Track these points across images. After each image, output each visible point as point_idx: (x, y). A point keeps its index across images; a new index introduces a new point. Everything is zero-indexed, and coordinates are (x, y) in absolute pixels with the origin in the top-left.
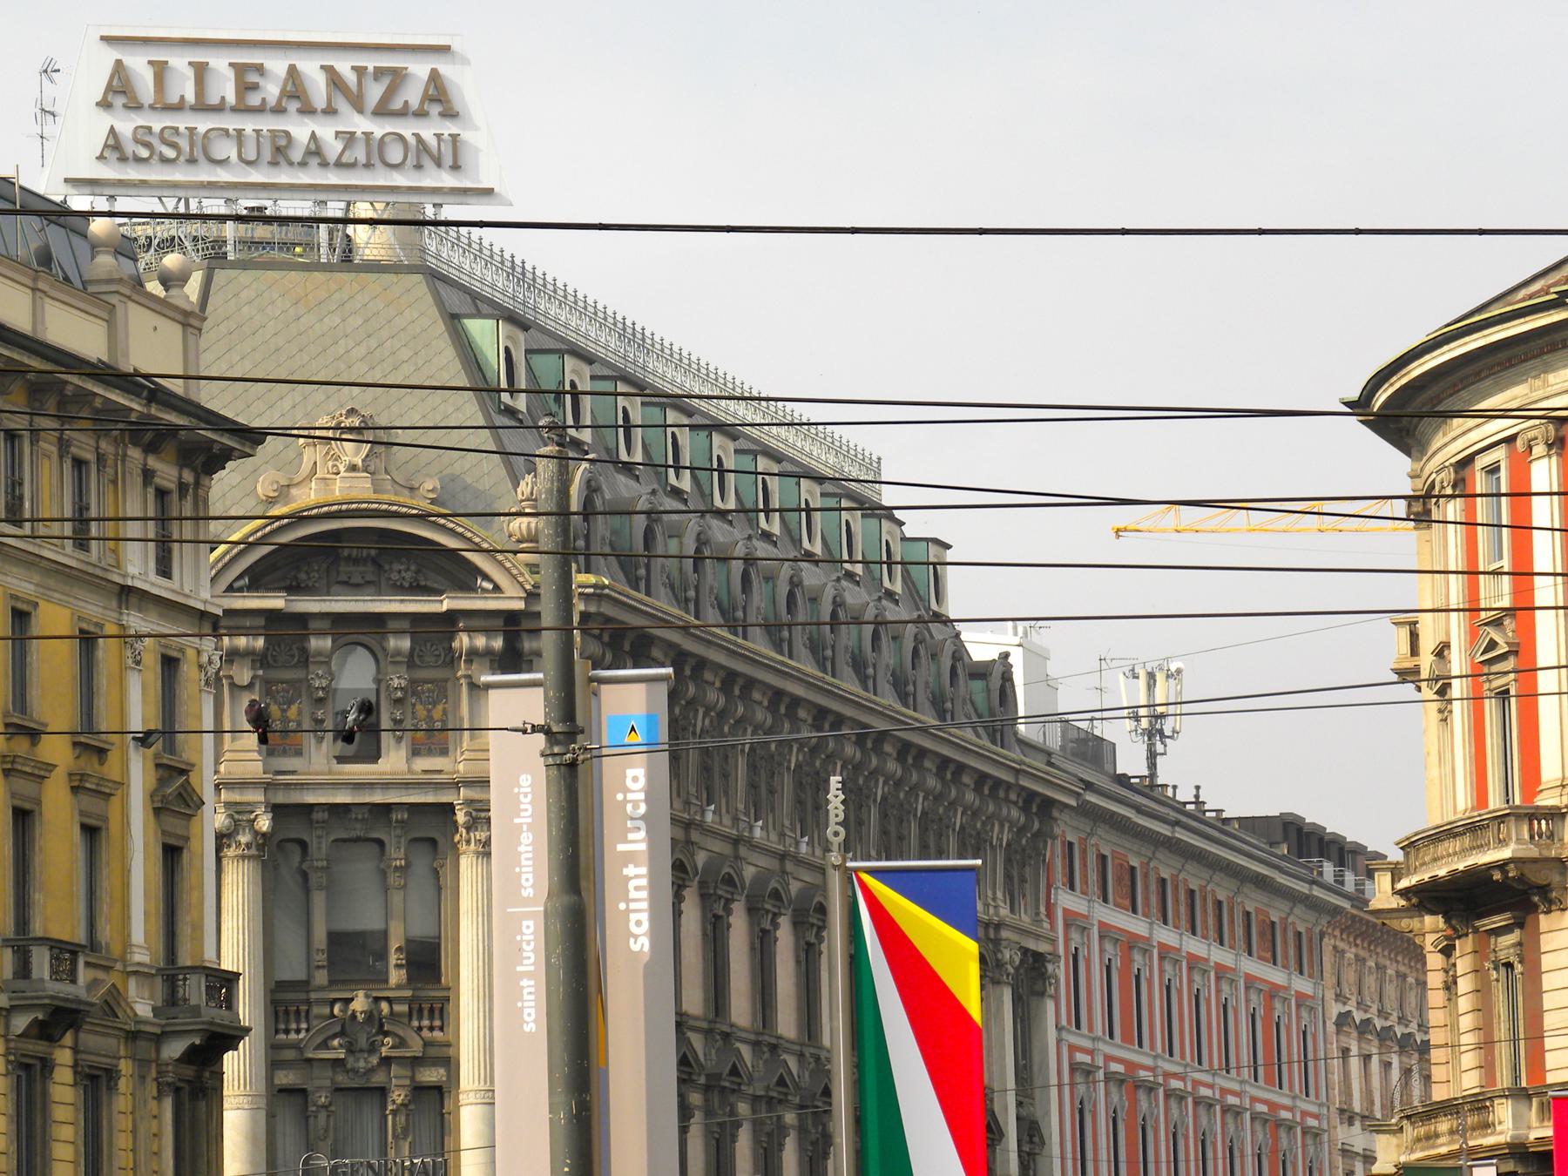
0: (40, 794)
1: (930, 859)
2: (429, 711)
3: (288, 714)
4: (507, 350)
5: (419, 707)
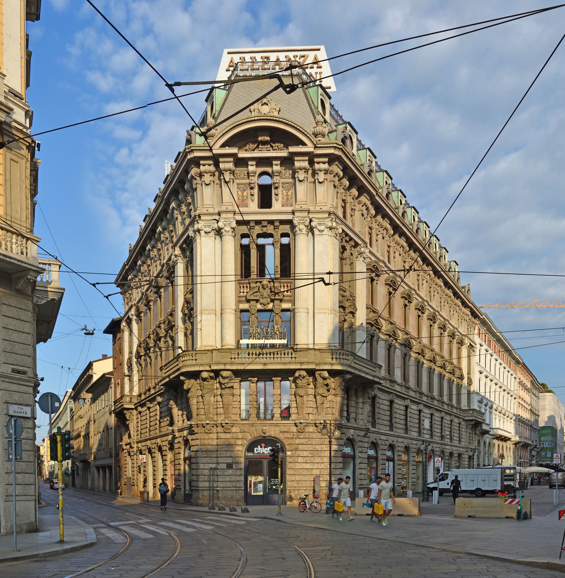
0: (27, 28)
1: (295, 46)
2: (287, 193)
3: (244, 194)
4: (425, 231)
5: (284, 191)
